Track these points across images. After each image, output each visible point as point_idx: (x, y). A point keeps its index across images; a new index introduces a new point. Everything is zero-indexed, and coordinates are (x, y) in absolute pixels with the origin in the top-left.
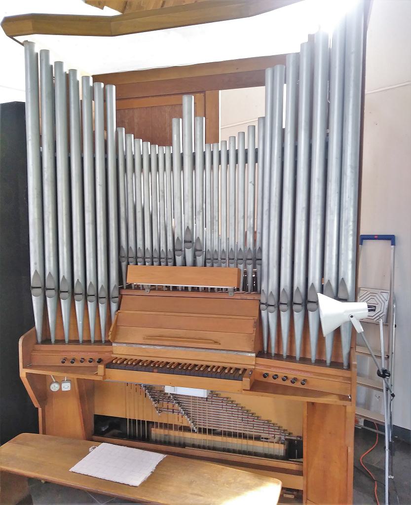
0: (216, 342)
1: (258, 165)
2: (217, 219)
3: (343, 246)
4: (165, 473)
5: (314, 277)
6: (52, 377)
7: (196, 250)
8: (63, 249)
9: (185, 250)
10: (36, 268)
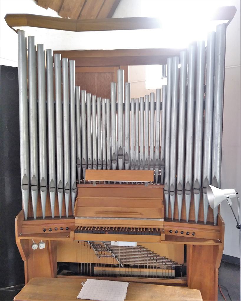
0: (141, 214)
1: (145, 112)
2: (138, 142)
3: (214, 158)
4: (134, 293)
5: (197, 175)
6: (33, 241)
7: (125, 160)
8: (42, 160)
9: (119, 159)
10: (24, 172)
